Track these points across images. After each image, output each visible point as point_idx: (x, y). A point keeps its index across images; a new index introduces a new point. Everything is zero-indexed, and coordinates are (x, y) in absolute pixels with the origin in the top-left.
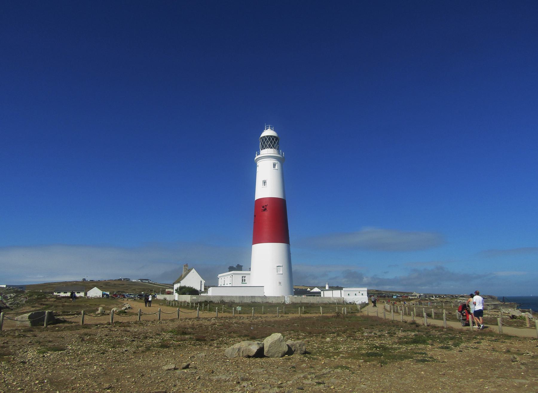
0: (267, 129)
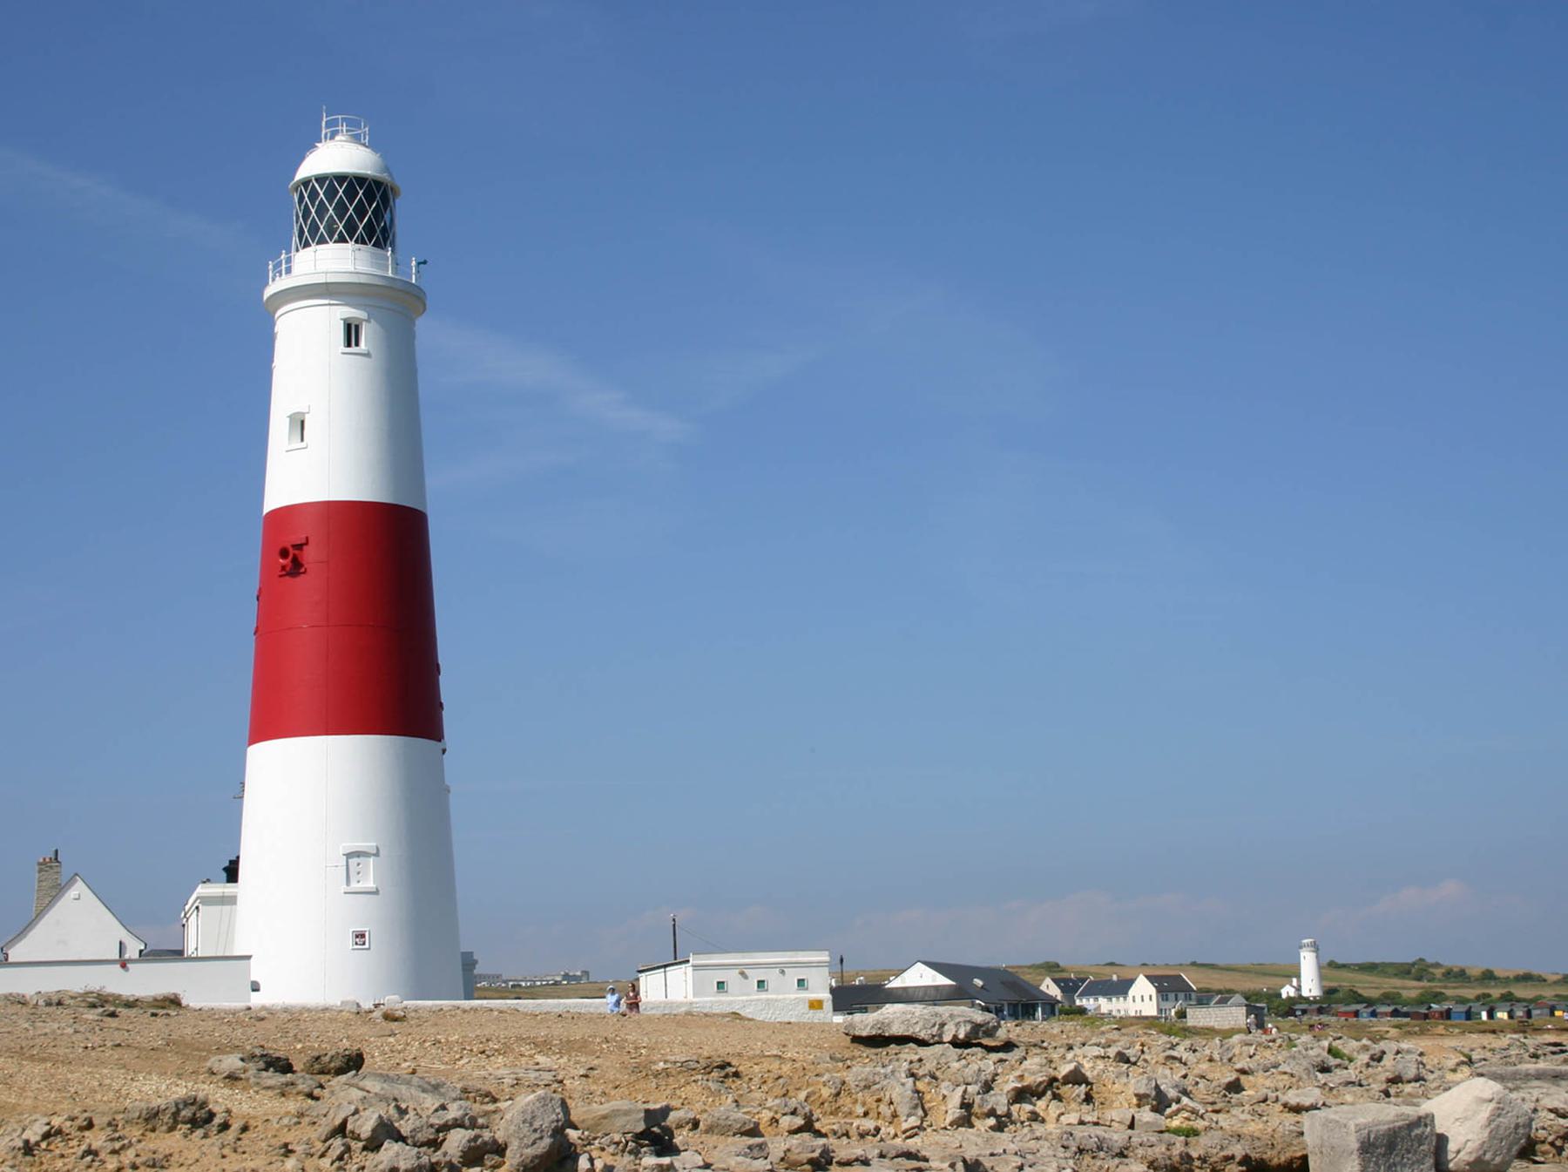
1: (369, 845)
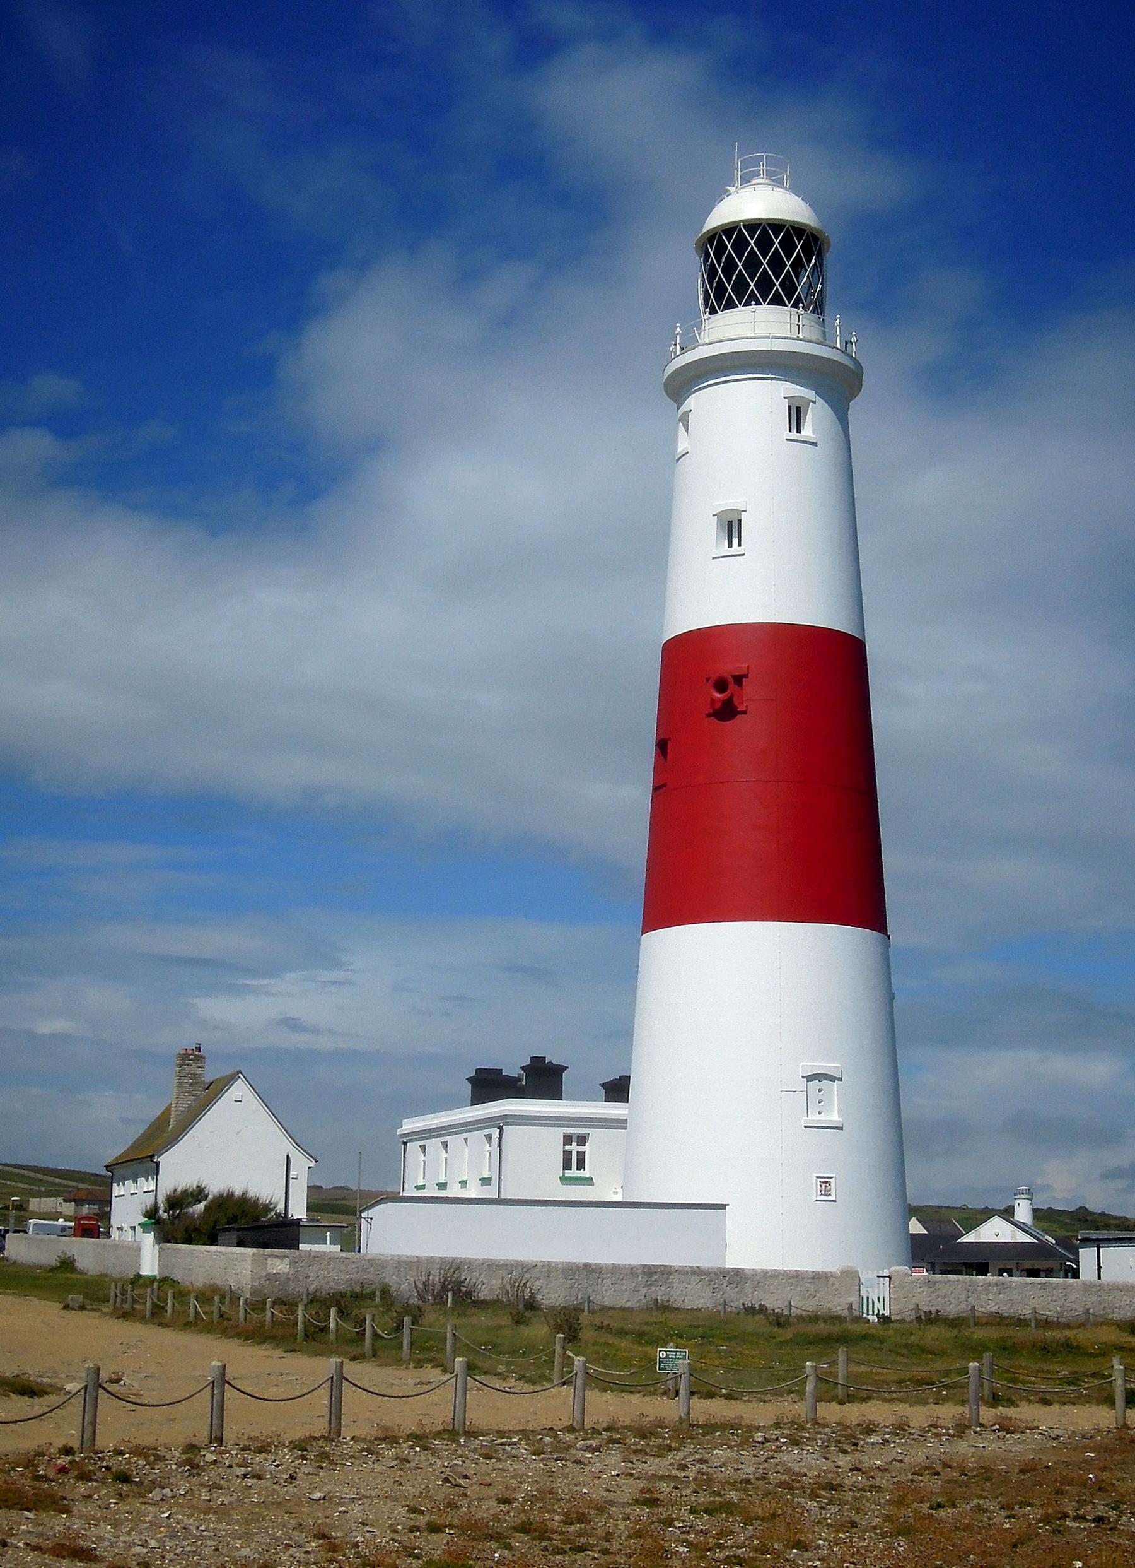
0: (746, 180)
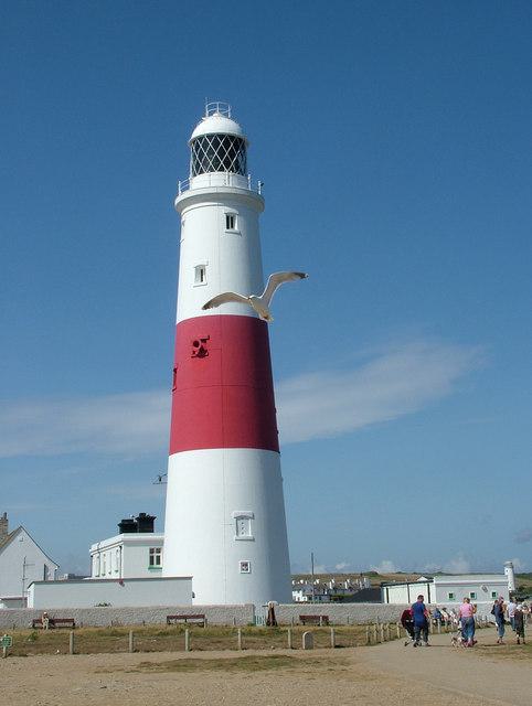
0: (211, 114)
1: (248, 512)
